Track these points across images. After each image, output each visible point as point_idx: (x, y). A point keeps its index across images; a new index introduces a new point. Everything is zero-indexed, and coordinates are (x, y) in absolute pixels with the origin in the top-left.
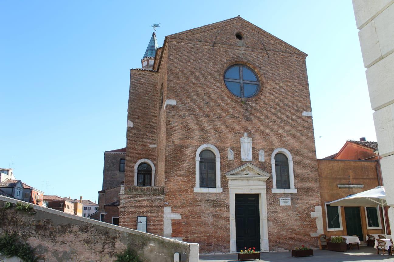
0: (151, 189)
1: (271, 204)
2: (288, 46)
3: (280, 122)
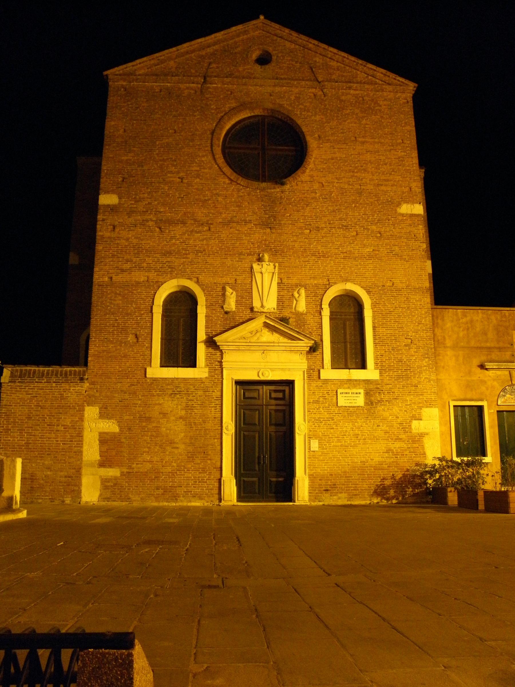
3: (346, 228)
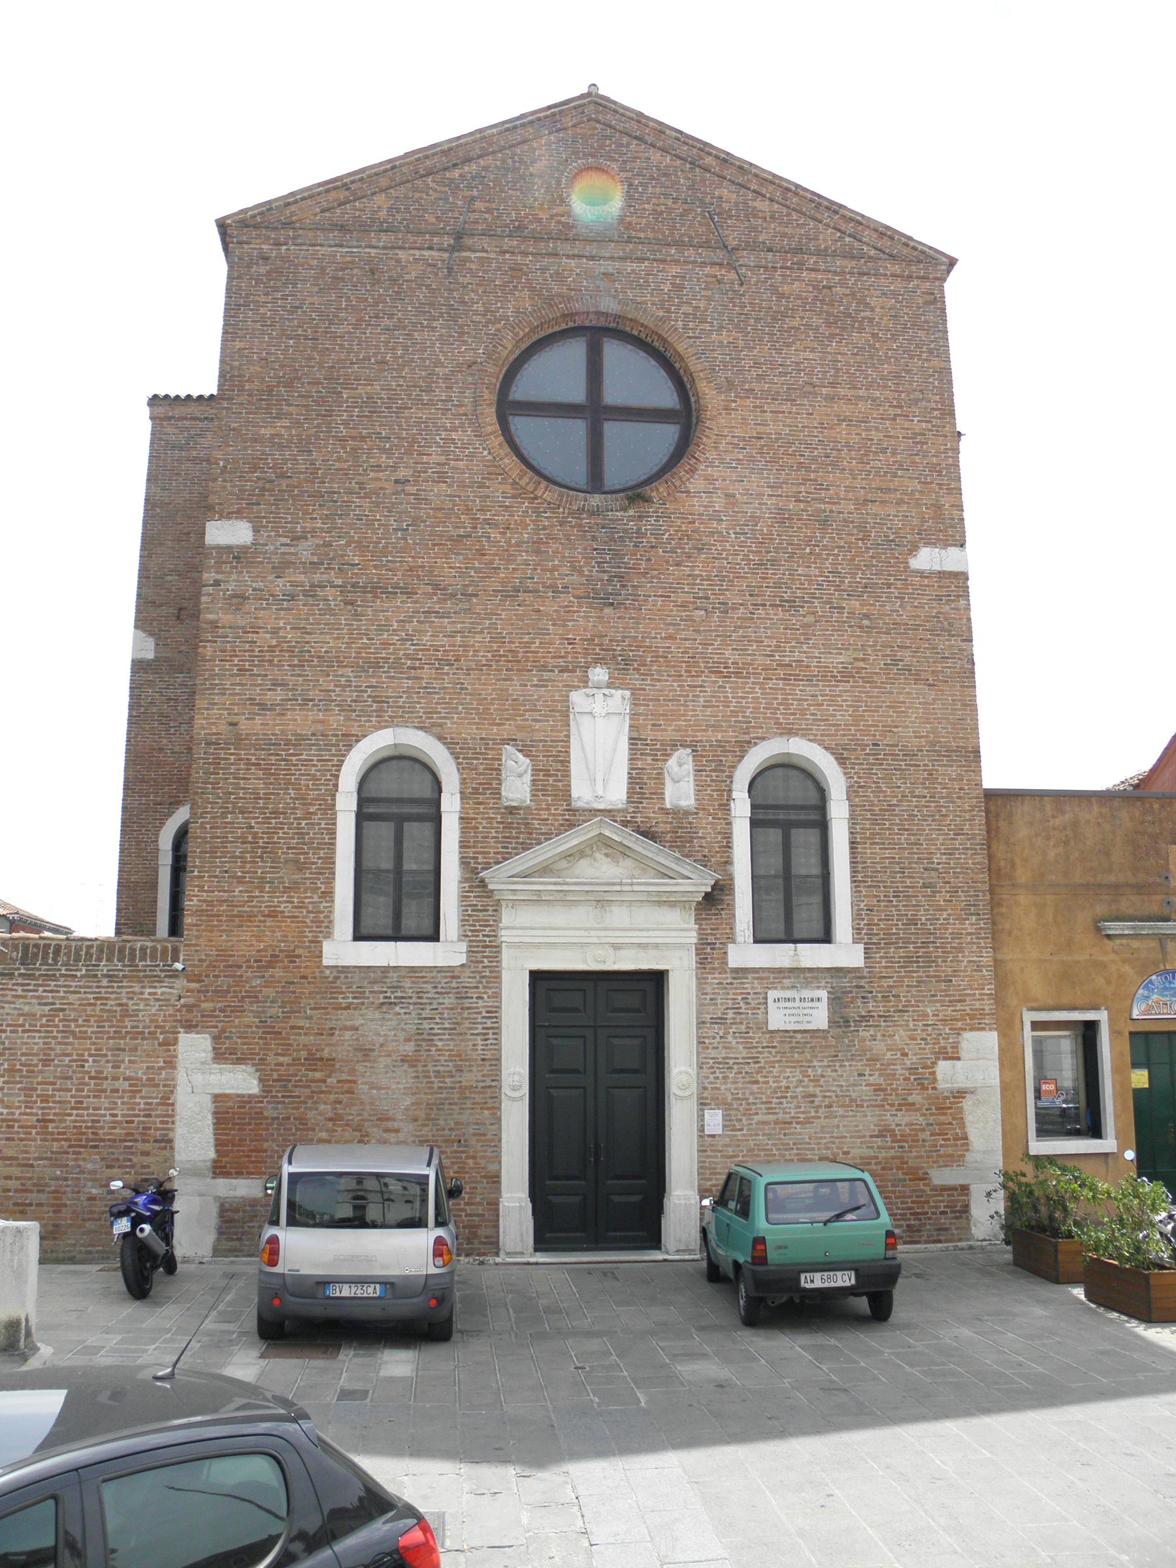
0: (154, 949)
1: (720, 1021)
2: (851, 219)
3: (791, 605)
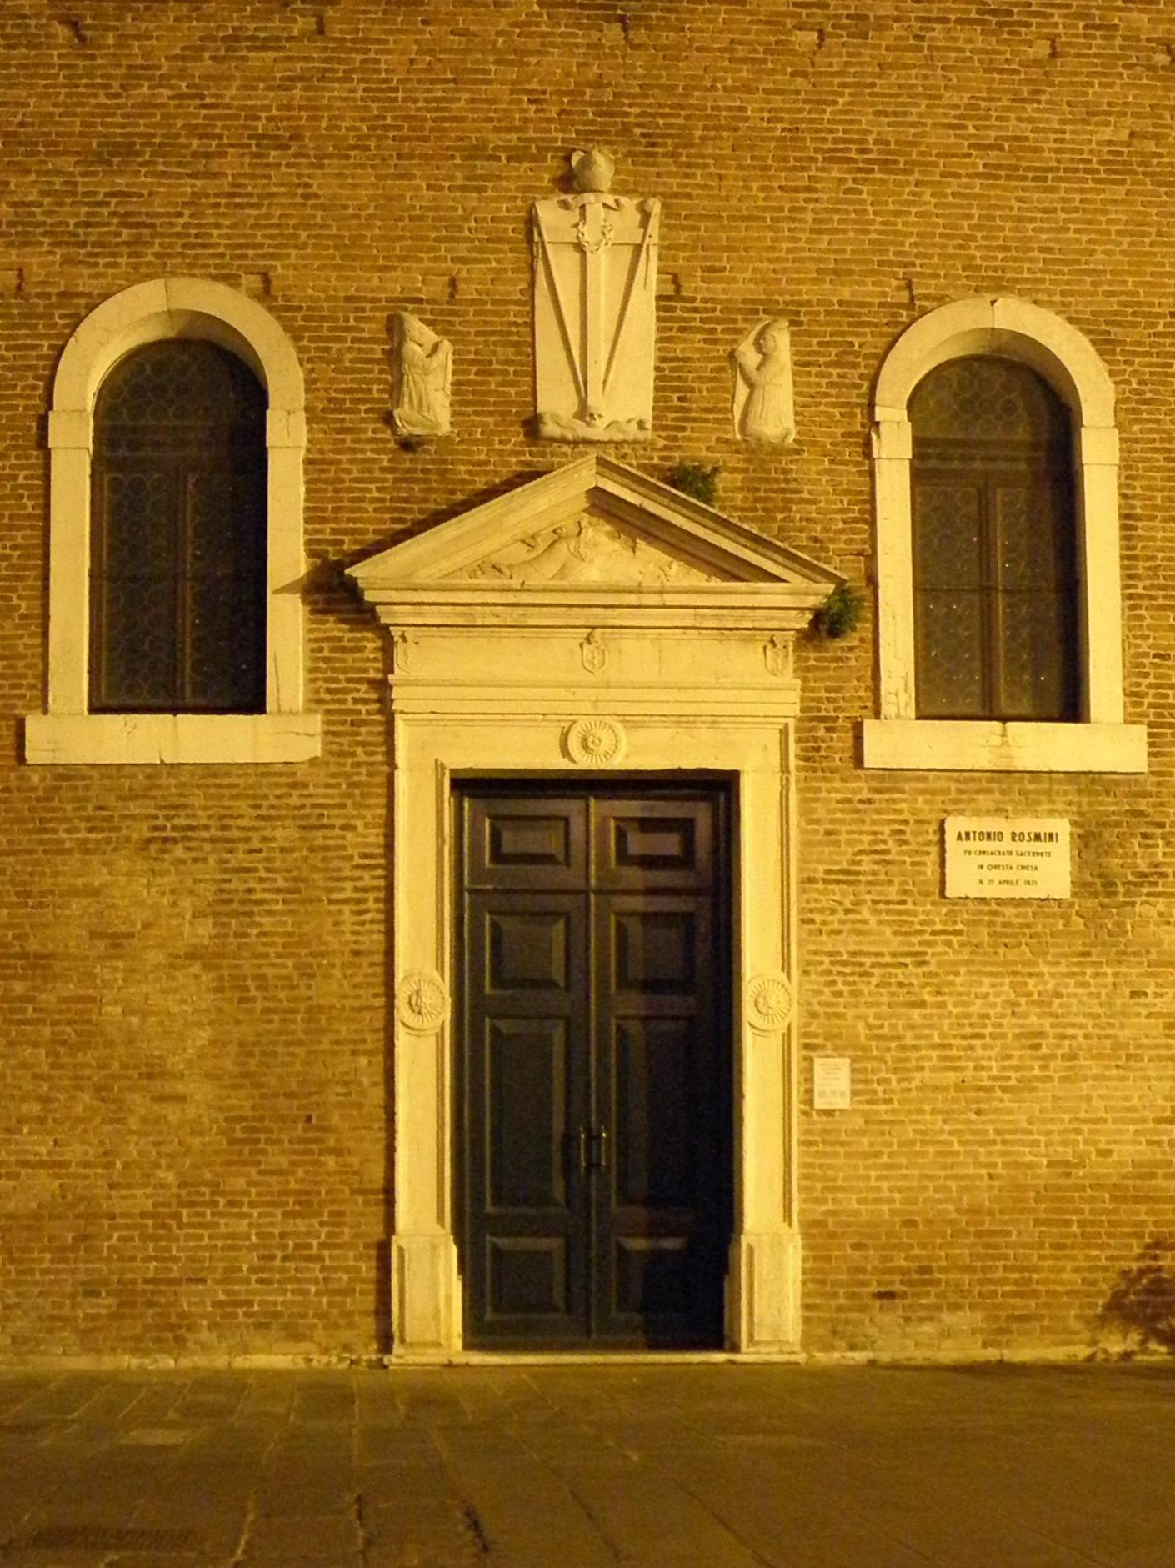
1: (847, 876)
